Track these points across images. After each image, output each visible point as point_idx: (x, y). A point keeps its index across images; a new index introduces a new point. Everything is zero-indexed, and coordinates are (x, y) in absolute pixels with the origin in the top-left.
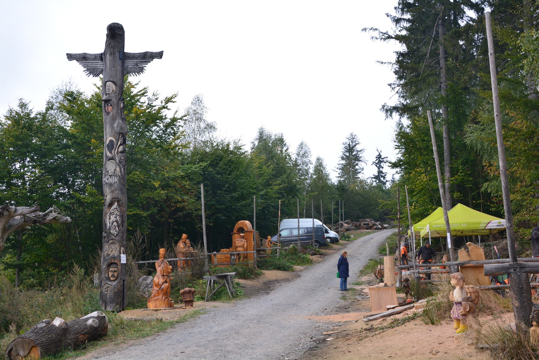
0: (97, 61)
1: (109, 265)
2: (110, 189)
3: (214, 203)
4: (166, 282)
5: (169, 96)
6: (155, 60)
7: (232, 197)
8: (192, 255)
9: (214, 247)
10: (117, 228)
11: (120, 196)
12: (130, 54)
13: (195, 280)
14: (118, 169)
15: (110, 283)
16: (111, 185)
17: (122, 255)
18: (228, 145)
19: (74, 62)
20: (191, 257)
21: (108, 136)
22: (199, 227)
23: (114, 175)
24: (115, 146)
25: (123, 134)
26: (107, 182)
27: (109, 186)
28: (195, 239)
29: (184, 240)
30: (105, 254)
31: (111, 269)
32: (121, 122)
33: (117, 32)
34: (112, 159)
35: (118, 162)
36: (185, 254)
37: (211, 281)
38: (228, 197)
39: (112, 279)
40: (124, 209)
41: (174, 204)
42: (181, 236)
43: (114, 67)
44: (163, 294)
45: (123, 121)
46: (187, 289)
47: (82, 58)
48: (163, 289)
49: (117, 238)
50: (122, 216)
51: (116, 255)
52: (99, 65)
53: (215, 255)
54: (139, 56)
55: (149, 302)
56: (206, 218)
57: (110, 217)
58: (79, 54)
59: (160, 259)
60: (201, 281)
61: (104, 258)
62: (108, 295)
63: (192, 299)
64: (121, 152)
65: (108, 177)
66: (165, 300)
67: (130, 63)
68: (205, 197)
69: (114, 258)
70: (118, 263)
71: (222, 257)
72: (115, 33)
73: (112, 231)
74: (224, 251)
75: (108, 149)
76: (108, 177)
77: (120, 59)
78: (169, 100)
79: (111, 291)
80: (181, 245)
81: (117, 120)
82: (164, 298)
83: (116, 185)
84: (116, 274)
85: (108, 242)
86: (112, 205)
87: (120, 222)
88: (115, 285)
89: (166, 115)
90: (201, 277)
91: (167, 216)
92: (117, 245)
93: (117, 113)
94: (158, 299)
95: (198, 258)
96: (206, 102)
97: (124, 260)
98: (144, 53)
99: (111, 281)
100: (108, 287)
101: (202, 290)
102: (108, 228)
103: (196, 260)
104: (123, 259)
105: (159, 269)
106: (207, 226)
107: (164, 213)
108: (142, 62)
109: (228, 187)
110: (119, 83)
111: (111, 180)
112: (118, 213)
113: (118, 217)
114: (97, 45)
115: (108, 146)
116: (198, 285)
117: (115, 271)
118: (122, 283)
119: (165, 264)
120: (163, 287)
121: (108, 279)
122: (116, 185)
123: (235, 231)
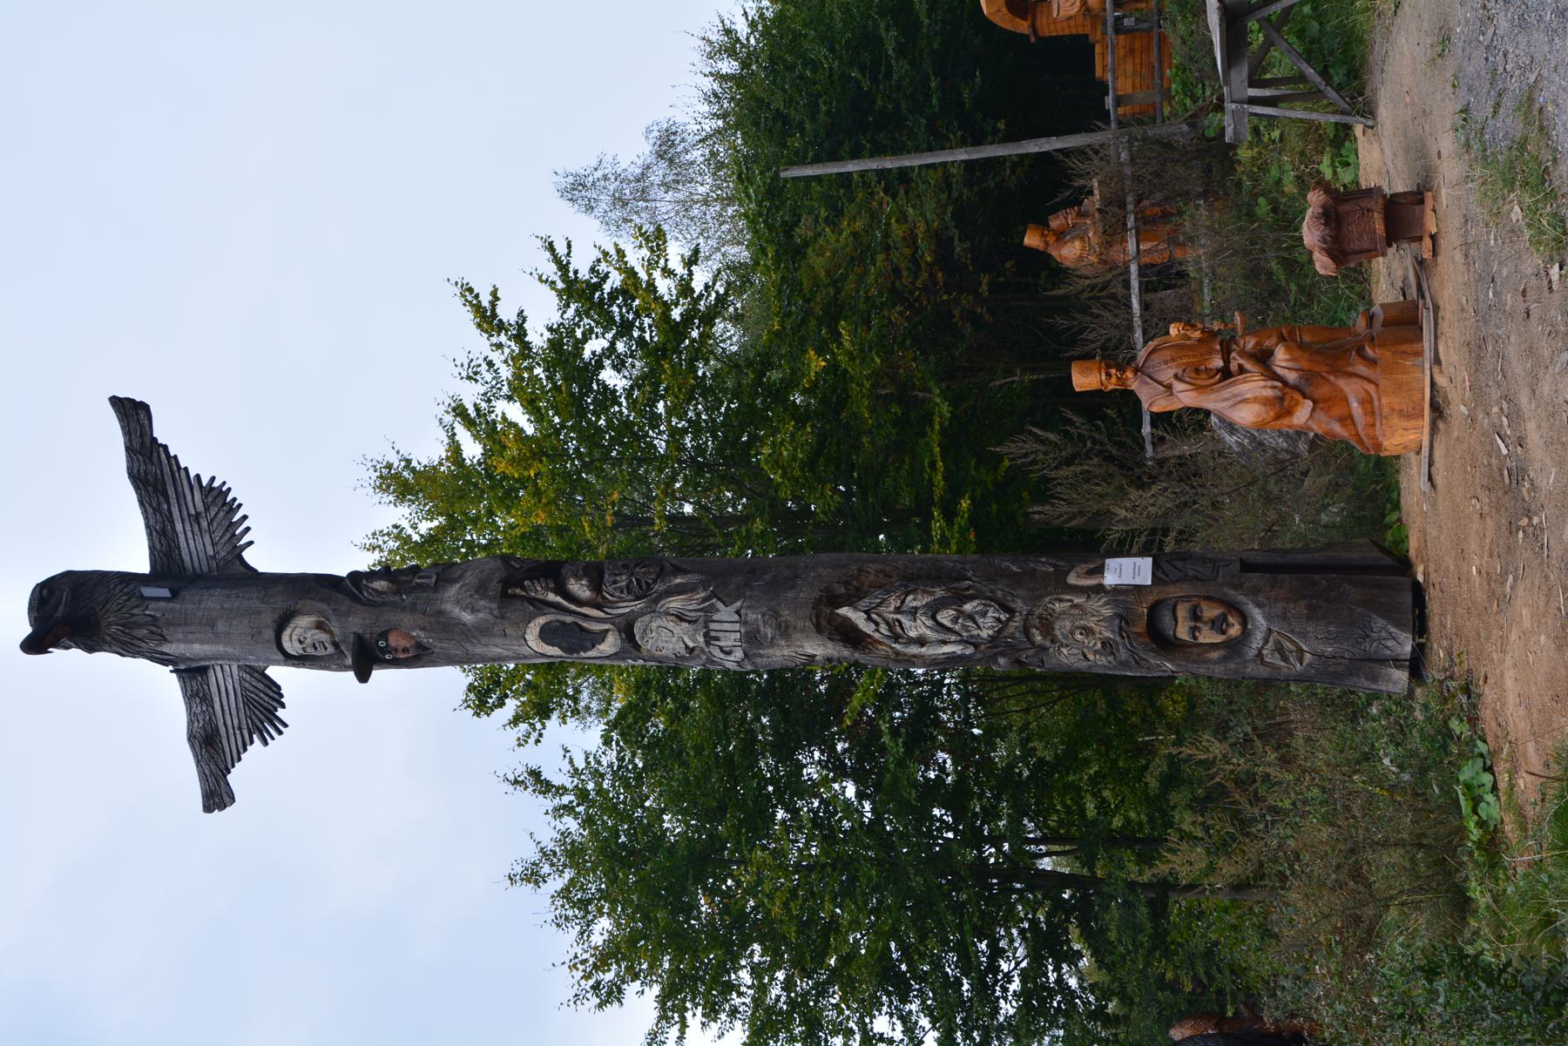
0: (214, 689)
1: (1163, 643)
2: (772, 644)
3: (924, 121)
4: (1263, 358)
5: (467, 317)
6: (161, 433)
7: (901, 51)
8: (1114, 202)
9: (1086, 108)
10: (968, 607)
11: (806, 593)
12: (152, 548)
13: (1239, 184)
14: (675, 603)
15: (1257, 641)
16: (752, 639)
17: (1110, 579)
18: (720, 77)
19: (237, 778)
20: (1122, 205)
21: (525, 651)
22: (1013, 171)
23: (703, 620)
24: (569, 619)
25: (507, 582)
26: (739, 654)
27: (760, 645)
28: (1049, 187)
29: (1051, 239)
30: (1102, 660)
31: (1183, 633)
32: (453, 590)
33: (59, 613)
34: (627, 630)
35: (638, 605)
36: (1113, 233)
37: (1253, 101)
38: (900, 68)
39: (1235, 630)
40: (872, 567)
41: (924, 275)
42: (1030, 250)
43: (212, 624)
44: (1337, 371)
45: (453, 581)
46: (1311, 234)
47: (214, 753)
48: (1309, 376)
49: (1019, 604)
50: (911, 581)
51: (1107, 612)
52: (225, 680)
53: (1119, 101)
54: (157, 510)
55: (1378, 446)
56: (978, 141)
57: (912, 641)
58: (198, 763)
59: (1134, 385)
60: (1244, 154)
61: (1124, 664)
62: (1320, 648)
63: (1377, 207)
64: (596, 587)
65: (717, 653)
66: (1373, 362)
67: (195, 547)
68: (897, 150)
69: (1123, 620)
70: (1151, 598)
71: (1129, 67)
72: (72, 613)
73: (985, 634)
74: (1103, 66)
75: (586, 650)
76: (717, 653)
77: (175, 594)
78: (487, 320)
79: (1303, 635)
80: (1069, 252)
81: (448, 607)
82: (1361, 369)
83: (751, 616)
84: (1210, 612)
85: (1043, 649)
86: (854, 628)
87: (939, 592)
88: (1268, 618)
89: (550, 329)
90: (1219, 152)
91: (966, 301)
92: (1058, 606)
93: (413, 608)
94: (1367, 402)
95: (1128, 171)
96: (580, 162)
97: (1136, 570)
98: (137, 488)
99: (1246, 634)
100: (1279, 649)
101: (1294, 142)
102: (970, 650)
103: (1137, 179)
104: (1129, 571)
105: (1185, 397)
106: (1010, 138)
107: (957, 312)
108: (180, 497)
109: (862, 70)
110: (281, 603)
111: (731, 639)
112: (894, 603)
113: (911, 601)
114: (137, 698)
115: (569, 650)
116: (1264, 169)
117: (1195, 616)
118: (1255, 579)
119: (1155, 358)
120: (1292, 377)
121: (1234, 647)
122: (751, 616)
123: (1023, 27)
